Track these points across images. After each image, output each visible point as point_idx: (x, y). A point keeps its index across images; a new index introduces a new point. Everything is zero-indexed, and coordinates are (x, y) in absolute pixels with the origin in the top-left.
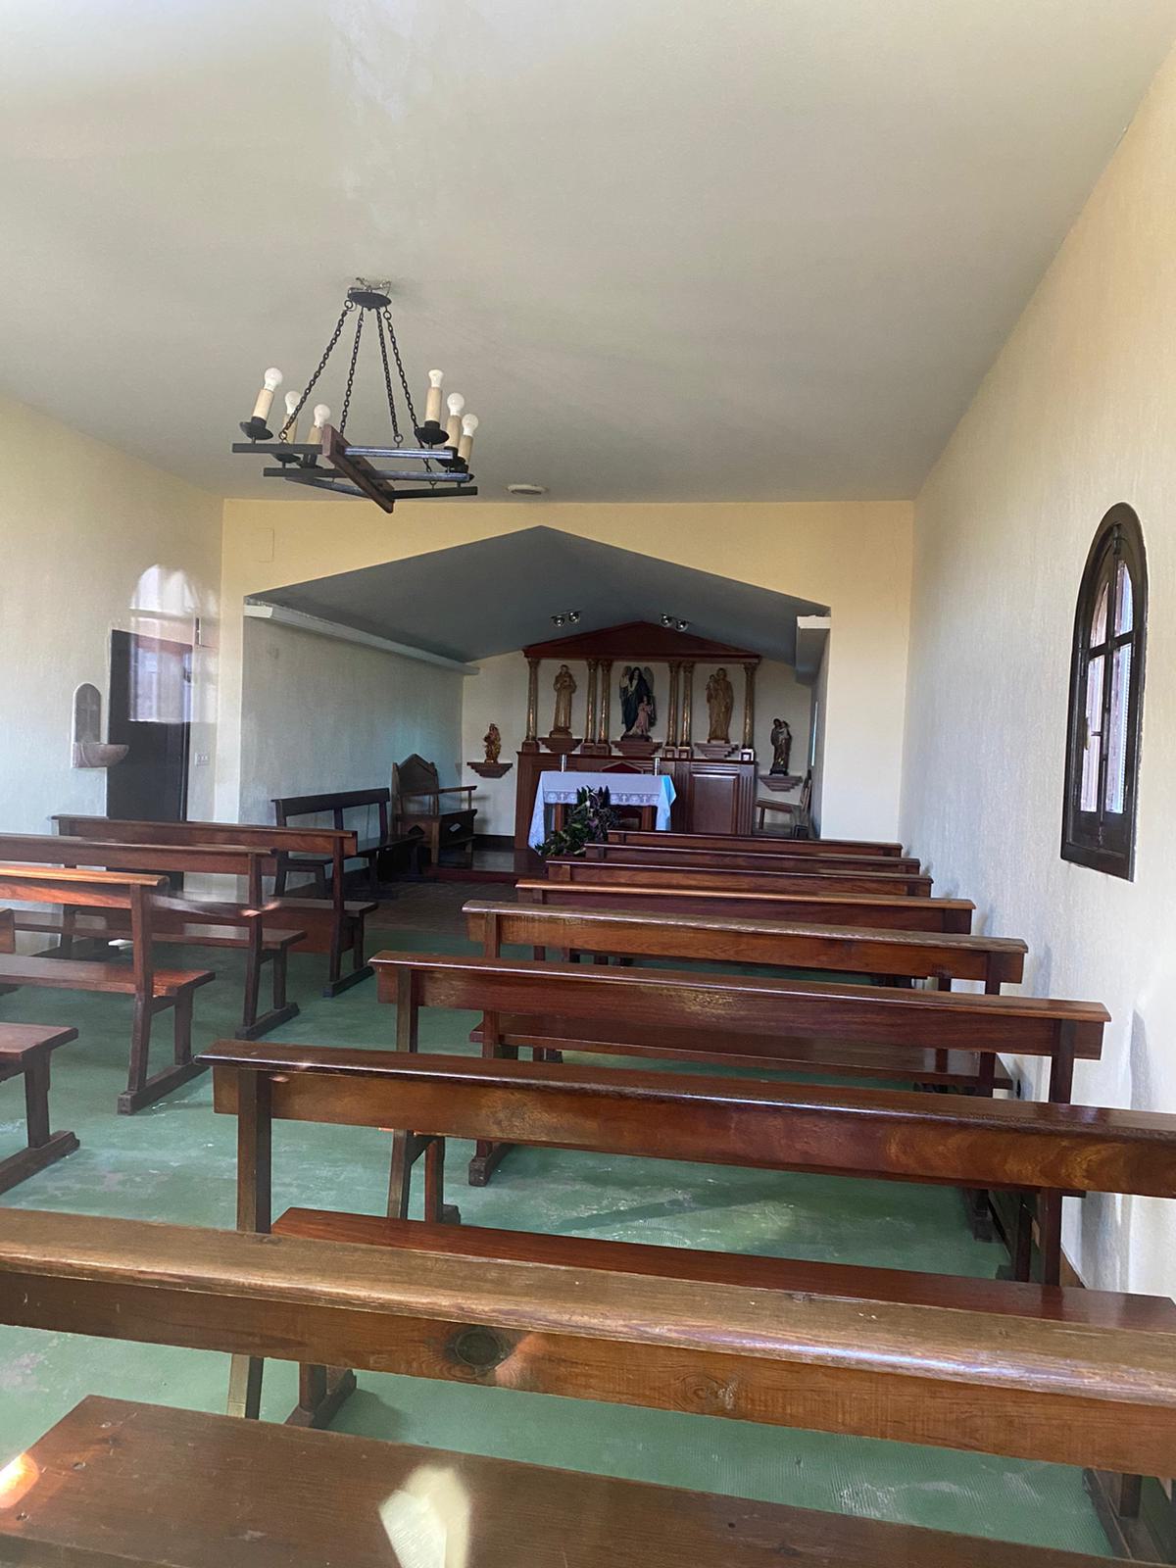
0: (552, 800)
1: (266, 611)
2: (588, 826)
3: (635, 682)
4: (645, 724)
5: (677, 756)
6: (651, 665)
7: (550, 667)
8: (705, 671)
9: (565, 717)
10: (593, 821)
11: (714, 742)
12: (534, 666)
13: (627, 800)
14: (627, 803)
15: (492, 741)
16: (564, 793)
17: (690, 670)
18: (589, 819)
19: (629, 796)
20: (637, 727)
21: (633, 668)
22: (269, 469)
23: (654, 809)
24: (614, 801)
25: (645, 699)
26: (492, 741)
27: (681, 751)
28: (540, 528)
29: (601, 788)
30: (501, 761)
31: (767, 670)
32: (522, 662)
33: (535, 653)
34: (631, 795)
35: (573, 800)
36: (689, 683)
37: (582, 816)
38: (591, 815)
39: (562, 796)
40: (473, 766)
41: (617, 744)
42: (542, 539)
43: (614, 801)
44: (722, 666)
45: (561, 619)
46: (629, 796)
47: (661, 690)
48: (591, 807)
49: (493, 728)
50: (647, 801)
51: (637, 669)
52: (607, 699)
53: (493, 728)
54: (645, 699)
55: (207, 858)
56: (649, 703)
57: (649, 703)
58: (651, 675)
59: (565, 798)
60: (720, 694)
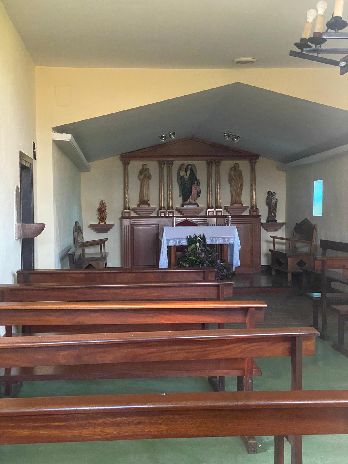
0: (172, 243)
1: (66, 137)
2: (199, 258)
3: (189, 173)
4: (196, 196)
5: (167, 215)
6: (195, 162)
7: (136, 166)
8: (227, 165)
9: (253, 197)
10: (201, 254)
11: (235, 205)
12: (126, 165)
13: (179, 242)
14: (228, 243)
15: (102, 211)
16: (215, 238)
17: (218, 164)
18: (199, 253)
19: (217, 239)
20: (191, 199)
21: (186, 165)
22: (292, 51)
23: (232, 246)
24: (208, 242)
25: (196, 183)
26: (102, 211)
27: (217, 212)
28: (238, 83)
29: (187, 237)
30: (108, 222)
31: (261, 163)
32: (116, 163)
33: (126, 158)
34: (218, 238)
35: (184, 243)
36: (217, 173)
37: (194, 252)
38: (200, 251)
39: (214, 240)
40: (92, 227)
41: (134, 210)
42: (236, 89)
43: (208, 242)
44: (191, 162)
45: (165, 137)
46: (217, 239)
47: (201, 175)
48: (199, 247)
49: (102, 204)
50: (228, 241)
51: (189, 165)
52: (170, 182)
53: (102, 204)
54: (196, 183)
55: (199, 288)
56: (197, 185)
57: (197, 185)
58: (196, 168)
59: (216, 241)
60: (235, 177)
